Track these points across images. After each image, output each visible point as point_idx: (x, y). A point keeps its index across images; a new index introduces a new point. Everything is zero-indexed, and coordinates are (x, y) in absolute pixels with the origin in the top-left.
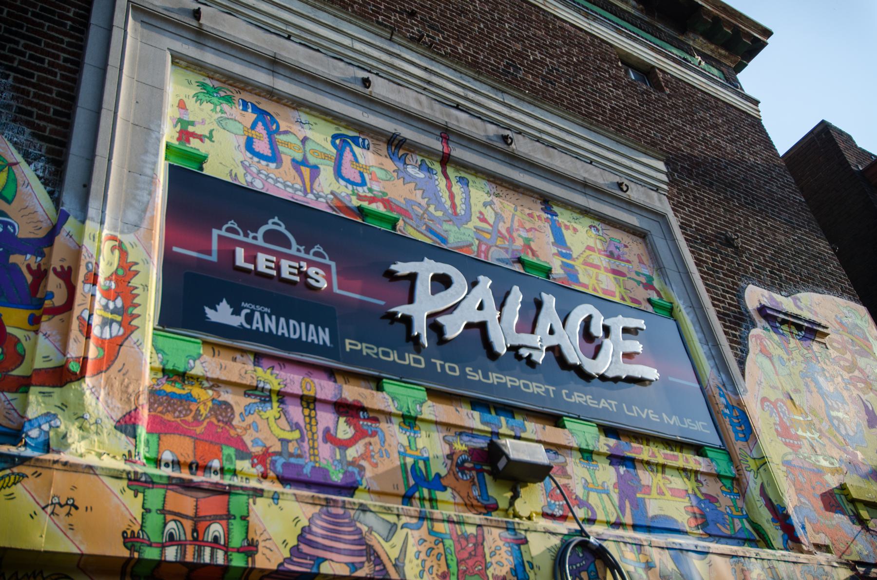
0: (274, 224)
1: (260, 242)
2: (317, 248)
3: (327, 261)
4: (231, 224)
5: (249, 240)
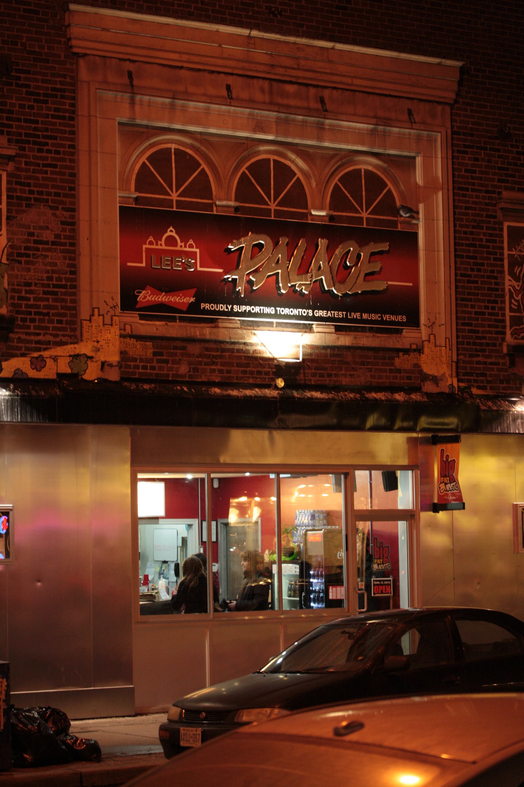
0: (171, 232)
1: (164, 247)
2: (191, 242)
3: (194, 250)
4: (151, 239)
5: (159, 247)
